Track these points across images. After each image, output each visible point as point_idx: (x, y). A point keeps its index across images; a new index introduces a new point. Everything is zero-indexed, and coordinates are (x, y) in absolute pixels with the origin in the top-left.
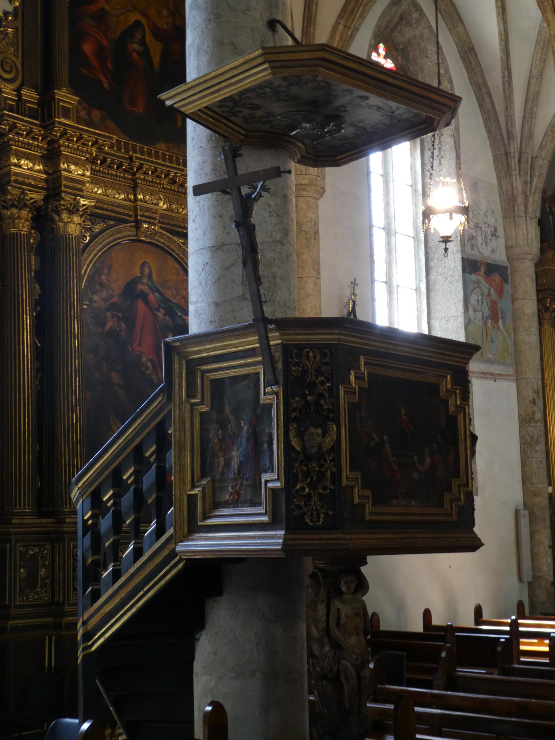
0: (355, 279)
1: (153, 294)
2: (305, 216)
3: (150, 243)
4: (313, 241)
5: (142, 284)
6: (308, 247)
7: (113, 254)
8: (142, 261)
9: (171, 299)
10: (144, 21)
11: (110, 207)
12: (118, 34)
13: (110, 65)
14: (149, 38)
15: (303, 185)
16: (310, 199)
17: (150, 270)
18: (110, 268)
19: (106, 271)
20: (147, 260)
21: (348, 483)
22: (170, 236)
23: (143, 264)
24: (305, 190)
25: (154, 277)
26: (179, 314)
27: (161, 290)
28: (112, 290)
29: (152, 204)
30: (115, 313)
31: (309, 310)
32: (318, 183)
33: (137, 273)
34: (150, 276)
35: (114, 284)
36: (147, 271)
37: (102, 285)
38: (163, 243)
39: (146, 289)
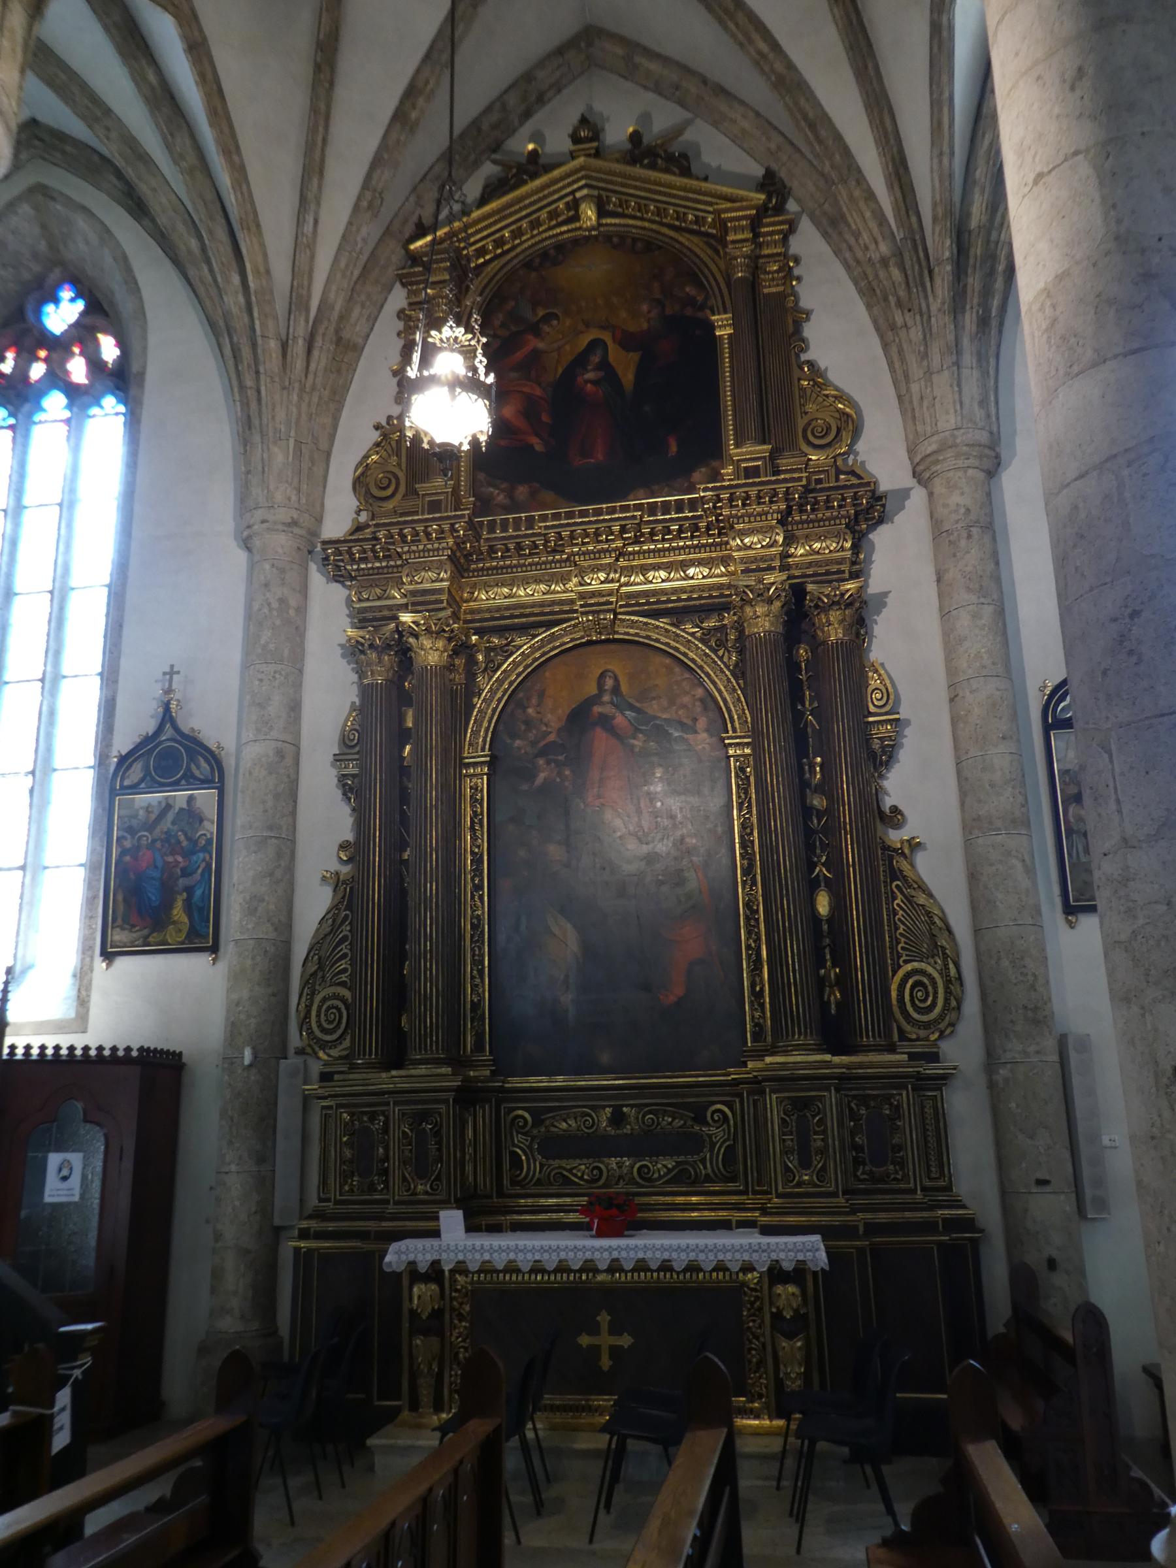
0: (156, 681)
1: (623, 714)
2: (946, 506)
3: (607, 641)
4: (963, 543)
5: (603, 704)
6: (955, 556)
7: (547, 674)
8: (600, 671)
9: (659, 714)
10: (606, 337)
11: (536, 610)
12: (560, 371)
13: (545, 418)
14: (615, 354)
15: (929, 455)
16: (951, 474)
17: (616, 680)
18: (542, 695)
19: (534, 701)
20: (609, 667)
21: (447, 1273)
22: (645, 620)
23: (602, 676)
24: (937, 462)
25: (624, 688)
26: (676, 734)
27: (637, 705)
28: (546, 725)
29: (704, 577)
30: (551, 757)
31: (965, 665)
32: (958, 441)
33: (592, 689)
34: (616, 690)
35: (549, 716)
36: (609, 683)
37: (528, 723)
38: (637, 635)
39: (607, 709)
